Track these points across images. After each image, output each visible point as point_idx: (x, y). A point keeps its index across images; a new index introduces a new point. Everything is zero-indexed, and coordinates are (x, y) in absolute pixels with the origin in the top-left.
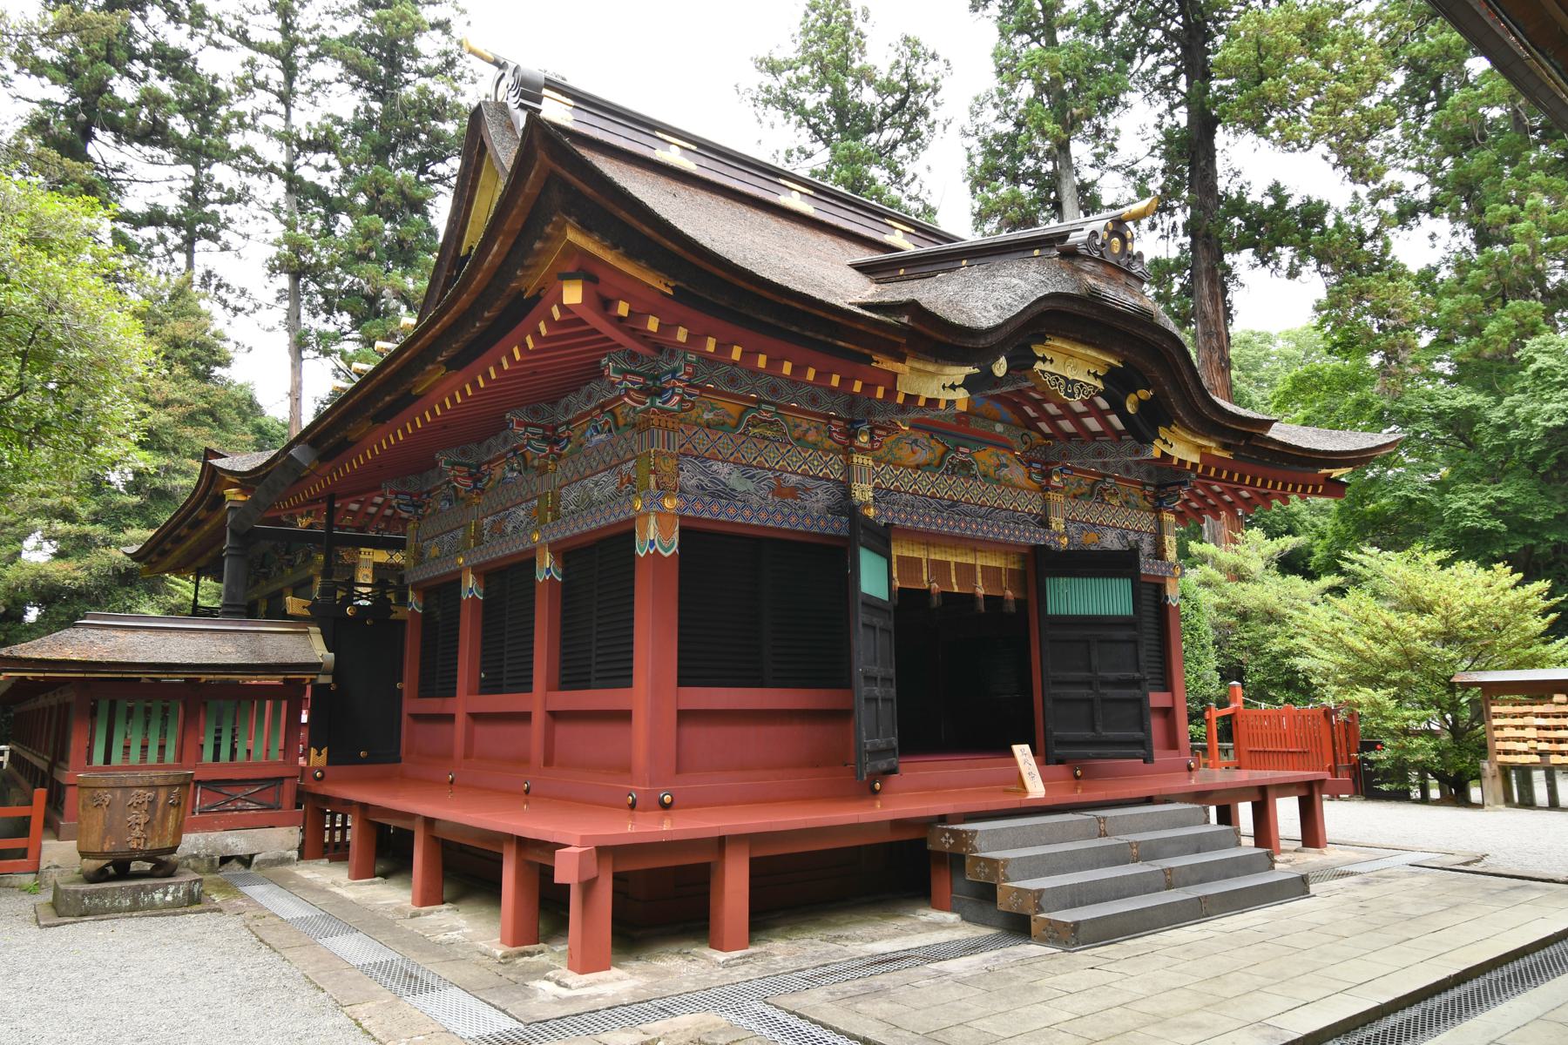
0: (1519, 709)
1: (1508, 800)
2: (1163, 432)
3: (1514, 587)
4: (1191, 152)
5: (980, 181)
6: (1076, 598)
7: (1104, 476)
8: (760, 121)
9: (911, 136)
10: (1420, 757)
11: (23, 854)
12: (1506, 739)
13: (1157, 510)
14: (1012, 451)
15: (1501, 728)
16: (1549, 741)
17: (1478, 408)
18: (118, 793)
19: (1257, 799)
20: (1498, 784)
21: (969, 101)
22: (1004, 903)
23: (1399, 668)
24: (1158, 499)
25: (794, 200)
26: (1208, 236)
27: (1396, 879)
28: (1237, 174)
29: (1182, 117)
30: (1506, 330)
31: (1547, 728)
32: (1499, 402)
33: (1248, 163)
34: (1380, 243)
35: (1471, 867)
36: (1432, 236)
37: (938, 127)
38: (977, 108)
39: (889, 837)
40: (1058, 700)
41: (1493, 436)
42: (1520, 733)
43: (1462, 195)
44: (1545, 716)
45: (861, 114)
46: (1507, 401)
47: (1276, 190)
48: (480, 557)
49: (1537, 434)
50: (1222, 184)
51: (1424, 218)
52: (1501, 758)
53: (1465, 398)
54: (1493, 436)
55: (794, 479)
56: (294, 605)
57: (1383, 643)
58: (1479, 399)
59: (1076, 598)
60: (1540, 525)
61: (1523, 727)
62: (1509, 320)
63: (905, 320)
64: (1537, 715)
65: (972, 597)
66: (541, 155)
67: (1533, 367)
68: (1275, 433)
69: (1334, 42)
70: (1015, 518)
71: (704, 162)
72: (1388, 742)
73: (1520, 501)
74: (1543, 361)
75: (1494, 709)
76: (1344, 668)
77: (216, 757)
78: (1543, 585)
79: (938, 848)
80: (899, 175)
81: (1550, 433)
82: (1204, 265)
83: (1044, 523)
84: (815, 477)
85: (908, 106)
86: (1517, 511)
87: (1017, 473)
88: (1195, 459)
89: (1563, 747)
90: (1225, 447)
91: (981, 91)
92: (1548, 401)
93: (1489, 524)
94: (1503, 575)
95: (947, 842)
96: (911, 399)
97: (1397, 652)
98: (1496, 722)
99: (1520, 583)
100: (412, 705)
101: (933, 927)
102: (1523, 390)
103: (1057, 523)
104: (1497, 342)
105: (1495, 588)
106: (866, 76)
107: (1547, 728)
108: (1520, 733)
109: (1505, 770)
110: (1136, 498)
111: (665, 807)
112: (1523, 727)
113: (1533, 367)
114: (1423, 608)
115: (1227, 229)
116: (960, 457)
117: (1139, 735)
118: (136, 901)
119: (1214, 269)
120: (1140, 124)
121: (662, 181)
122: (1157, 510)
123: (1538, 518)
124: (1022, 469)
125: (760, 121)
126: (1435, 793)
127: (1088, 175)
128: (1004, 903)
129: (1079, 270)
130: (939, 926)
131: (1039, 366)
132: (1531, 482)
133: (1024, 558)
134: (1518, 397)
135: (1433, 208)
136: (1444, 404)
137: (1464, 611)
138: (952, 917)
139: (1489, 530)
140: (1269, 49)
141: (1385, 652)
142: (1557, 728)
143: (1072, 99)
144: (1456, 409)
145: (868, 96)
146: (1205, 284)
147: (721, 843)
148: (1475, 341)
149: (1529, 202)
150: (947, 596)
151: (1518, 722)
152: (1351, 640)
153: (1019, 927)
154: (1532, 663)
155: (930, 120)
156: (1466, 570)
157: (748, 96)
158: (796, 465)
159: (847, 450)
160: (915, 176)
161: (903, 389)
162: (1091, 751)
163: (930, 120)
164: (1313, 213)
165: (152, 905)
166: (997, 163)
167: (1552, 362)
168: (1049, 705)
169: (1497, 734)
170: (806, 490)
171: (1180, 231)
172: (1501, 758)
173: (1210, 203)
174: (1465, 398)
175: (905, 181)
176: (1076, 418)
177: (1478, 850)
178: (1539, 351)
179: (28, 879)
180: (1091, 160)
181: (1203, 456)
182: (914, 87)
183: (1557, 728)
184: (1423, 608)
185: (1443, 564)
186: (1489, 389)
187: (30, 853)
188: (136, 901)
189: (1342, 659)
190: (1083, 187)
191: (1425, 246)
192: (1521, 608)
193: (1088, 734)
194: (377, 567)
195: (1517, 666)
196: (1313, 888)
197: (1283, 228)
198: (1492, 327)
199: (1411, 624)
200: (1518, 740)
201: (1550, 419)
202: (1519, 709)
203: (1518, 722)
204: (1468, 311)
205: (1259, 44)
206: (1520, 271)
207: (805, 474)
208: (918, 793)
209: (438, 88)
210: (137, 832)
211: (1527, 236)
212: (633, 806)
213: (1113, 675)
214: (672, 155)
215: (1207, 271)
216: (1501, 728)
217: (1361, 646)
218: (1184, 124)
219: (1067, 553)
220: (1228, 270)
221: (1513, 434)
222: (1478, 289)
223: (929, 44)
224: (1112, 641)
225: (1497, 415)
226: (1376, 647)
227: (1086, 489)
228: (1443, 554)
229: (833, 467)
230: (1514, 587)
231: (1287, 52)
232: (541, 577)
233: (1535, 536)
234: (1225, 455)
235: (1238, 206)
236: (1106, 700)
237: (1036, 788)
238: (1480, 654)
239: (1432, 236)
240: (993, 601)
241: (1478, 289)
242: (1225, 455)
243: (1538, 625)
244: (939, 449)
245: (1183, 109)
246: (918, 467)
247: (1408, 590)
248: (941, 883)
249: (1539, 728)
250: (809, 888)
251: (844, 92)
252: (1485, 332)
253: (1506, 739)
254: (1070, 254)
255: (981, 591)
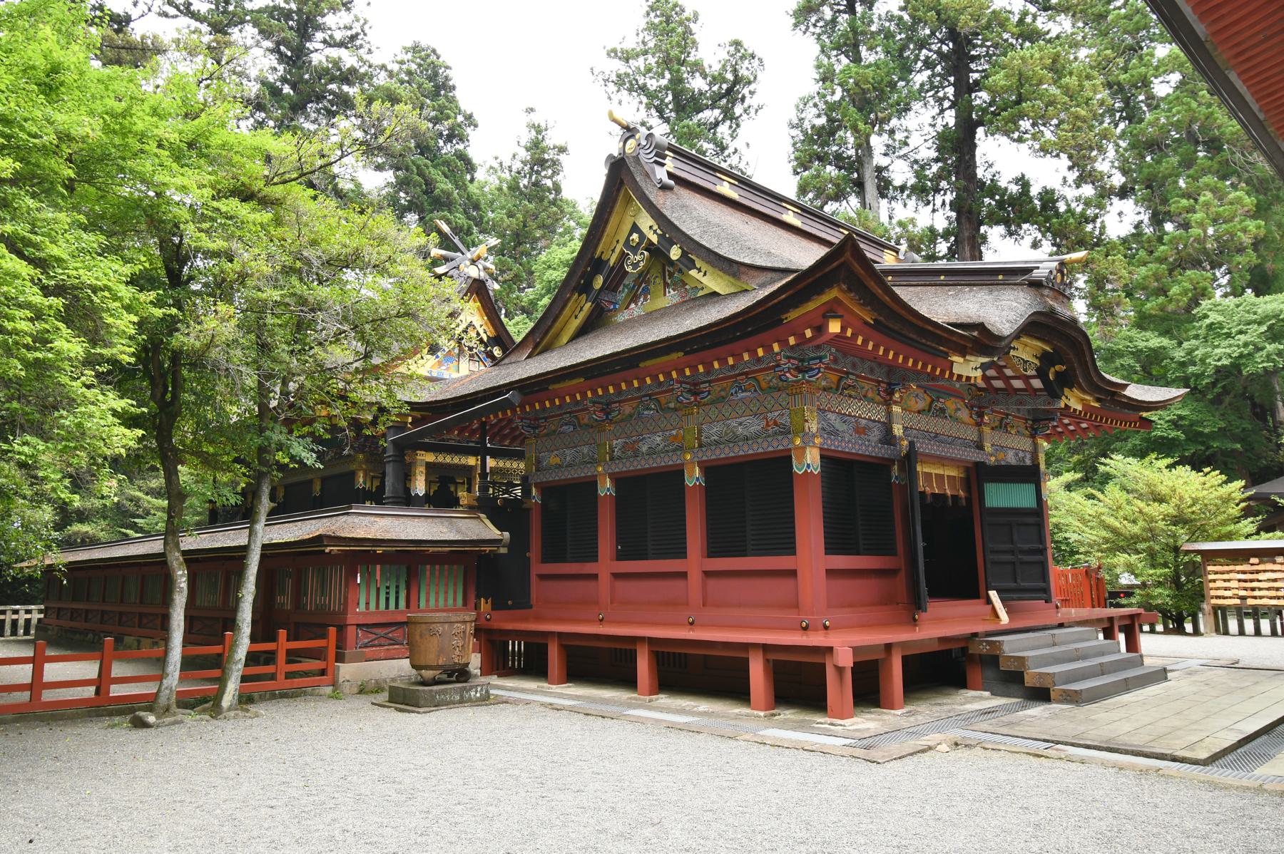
0: (1226, 568)
1: (1217, 631)
2: (1066, 391)
3: (1220, 485)
4: (957, 146)
5: (802, 163)
6: (1000, 496)
7: (1007, 415)
8: (610, 98)
9: (728, 115)
10: (1160, 602)
11: (323, 672)
12: (1218, 589)
13: (1033, 436)
14: (963, 400)
15: (1214, 581)
16: (1245, 589)
17: (1165, 348)
18: (446, 626)
19: (1106, 626)
20: (1211, 619)
21: (796, 101)
22: (1029, 681)
23: (1145, 540)
24: (1033, 429)
25: (790, 217)
26: (970, 212)
27: (1200, 676)
28: (991, 166)
29: (950, 118)
30: (1185, 292)
31: (1245, 581)
32: (1180, 344)
33: (1002, 158)
34: (1098, 225)
35: (1234, 665)
36: (1120, 214)
37: (752, 111)
38: (801, 106)
39: (936, 647)
40: (994, 563)
41: (1176, 370)
42: (1227, 584)
43: (1151, 189)
44: (1244, 572)
45: (689, 95)
46: (1186, 345)
47: (1023, 182)
48: (619, 468)
49: (1210, 371)
50: (980, 173)
51: (1115, 200)
52: (1214, 601)
53: (1154, 341)
54: (1176, 370)
55: (864, 422)
56: (463, 495)
57: (1134, 522)
58: (1165, 342)
59: (1000, 496)
60: (1207, 435)
61: (1229, 580)
62: (1188, 285)
63: (975, 334)
64: (1238, 572)
65: (944, 496)
66: (848, 254)
67: (1208, 321)
68: (1128, 392)
69: (1071, 74)
70: (965, 444)
71: (742, 192)
72: (1138, 591)
73: (1194, 418)
74: (1214, 317)
75: (1210, 568)
76: (1106, 541)
77: (387, 606)
78: (1240, 483)
79: (977, 652)
80: (723, 148)
81: (1218, 370)
82: (967, 234)
83: (980, 447)
84: (874, 421)
85: (730, 93)
86: (1191, 425)
87: (964, 414)
88: (1079, 408)
89: (1280, 594)
90: (1098, 400)
91: (805, 94)
92: (1217, 347)
93: (1173, 434)
94: (1216, 477)
95: (984, 649)
96: (960, 377)
97: (1144, 529)
98: (1211, 577)
99: (1226, 482)
100: (537, 568)
101: (974, 701)
102: (1196, 337)
103: (988, 447)
104: (1178, 301)
105: (1208, 485)
106: (697, 68)
107: (1245, 581)
108: (1227, 584)
109: (1216, 608)
110: (1022, 430)
111: (826, 628)
112: (1229, 580)
113: (1208, 321)
114: (1160, 499)
115: (978, 205)
116: (940, 405)
117: (1042, 585)
118: (462, 697)
119: (974, 237)
120: (922, 125)
121: (747, 217)
122: (1033, 436)
123: (1207, 431)
124: (967, 411)
125: (610, 98)
126: (1160, 628)
127: (884, 162)
128: (1029, 681)
129: (1042, 295)
130: (982, 698)
131: (693, 273)
132: (1202, 404)
133: (967, 470)
134: (1193, 342)
135: (1123, 193)
136: (1141, 345)
137: (1190, 502)
138: (987, 694)
139: (1173, 439)
140: (1028, 79)
141: (1136, 529)
142: (1252, 581)
143: (871, 102)
144: (1150, 349)
145: (698, 84)
146: (967, 248)
147: (888, 647)
148: (1161, 299)
149: (1202, 199)
150: (933, 495)
151: (1226, 576)
152: (1111, 521)
153: (1041, 695)
154: (1229, 536)
155: (746, 105)
156: (1184, 471)
157: (600, 77)
158: (859, 409)
159: (888, 403)
160: (736, 150)
161: (956, 370)
162: (1015, 596)
163: (746, 105)
164: (1048, 198)
165: (470, 700)
166: (813, 147)
167: (1221, 318)
168: (989, 566)
169: (1211, 585)
170: (870, 429)
171: (948, 207)
172: (1214, 601)
173: (971, 187)
174: (1154, 341)
175: (726, 153)
176: (1007, 379)
177: (1236, 658)
178: (1210, 310)
179: (329, 690)
180: (883, 150)
181: (1084, 405)
182: (737, 80)
183: (1252, 581)
184: (1160, 499)
185: (1170, 467)
186: (1166, 333)
187: (329, 671)
188: (462, 697)
189: (1104, 533)
190: (879, 170)
191: (1120, 219)
192: (1227, 500)
193: (1013, 585)
194: (430, 467)
195: (1219, 539)
196: (1170, 675)
197: (1019, 208)
198: (1175, 290)
199: (1155, 510)
200: (1226, 589)
201: (1219, 360)
202: (1226, 568)
203: (1226, 576)
204: (1157, 278)
205: (1020, 74)
206: (1194, 249)
207: (869, 419)
208: (944, 622)
209: (348, 59)
210: (457, 652)
211: (1201, 225)
212: (805, 629)
213: (1026, 547)
214: (725, 189)
215: (969, 238)
216: (1214, 581)
217: (1117, 524)
218: (952, 122)
219: (996, 467)
220: (984, 239)
221: (1191, 369)
222: (1162, 260)
223: (749, 45)
224: (1027, 525)
225: (1179, 354)
226: (1129, 525)
227: (997, 423)
228: (1169, 461)
229: (878, 414)
230: (1220, 485)
231: (1040, 83)
232: (690, 482)
233: (1203, 443)
234: (1097, 405)
235: (993, 189)
236: (1023, 563)
237: (1004, 618)
238: (1199, 532)
239: (1120, 214)
240: (955, 497)
241: (1162, 260)
242: (1097, 405)
243: (1234, 511)
244: (928, 400)
245: (953, 112)
246: (919, 412)
247: (1149, 485)
248: (974, 674)
249: (1240, 581)
250: (939, 672)
251: (681, 81)
252: (1170, 293)
253: (1218, 589)
254: (1036, 285)
255: (948, 492)
